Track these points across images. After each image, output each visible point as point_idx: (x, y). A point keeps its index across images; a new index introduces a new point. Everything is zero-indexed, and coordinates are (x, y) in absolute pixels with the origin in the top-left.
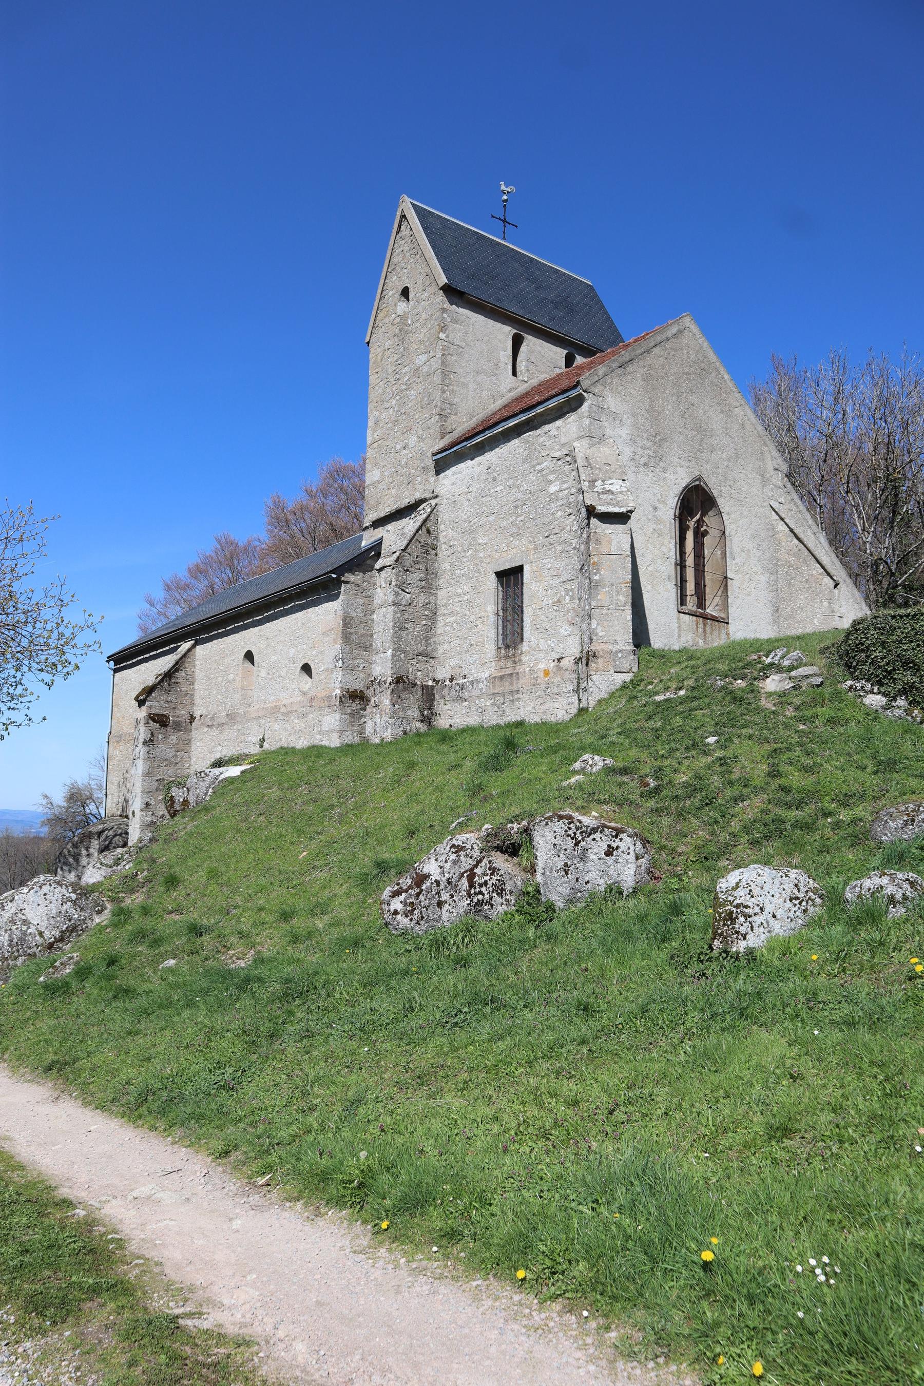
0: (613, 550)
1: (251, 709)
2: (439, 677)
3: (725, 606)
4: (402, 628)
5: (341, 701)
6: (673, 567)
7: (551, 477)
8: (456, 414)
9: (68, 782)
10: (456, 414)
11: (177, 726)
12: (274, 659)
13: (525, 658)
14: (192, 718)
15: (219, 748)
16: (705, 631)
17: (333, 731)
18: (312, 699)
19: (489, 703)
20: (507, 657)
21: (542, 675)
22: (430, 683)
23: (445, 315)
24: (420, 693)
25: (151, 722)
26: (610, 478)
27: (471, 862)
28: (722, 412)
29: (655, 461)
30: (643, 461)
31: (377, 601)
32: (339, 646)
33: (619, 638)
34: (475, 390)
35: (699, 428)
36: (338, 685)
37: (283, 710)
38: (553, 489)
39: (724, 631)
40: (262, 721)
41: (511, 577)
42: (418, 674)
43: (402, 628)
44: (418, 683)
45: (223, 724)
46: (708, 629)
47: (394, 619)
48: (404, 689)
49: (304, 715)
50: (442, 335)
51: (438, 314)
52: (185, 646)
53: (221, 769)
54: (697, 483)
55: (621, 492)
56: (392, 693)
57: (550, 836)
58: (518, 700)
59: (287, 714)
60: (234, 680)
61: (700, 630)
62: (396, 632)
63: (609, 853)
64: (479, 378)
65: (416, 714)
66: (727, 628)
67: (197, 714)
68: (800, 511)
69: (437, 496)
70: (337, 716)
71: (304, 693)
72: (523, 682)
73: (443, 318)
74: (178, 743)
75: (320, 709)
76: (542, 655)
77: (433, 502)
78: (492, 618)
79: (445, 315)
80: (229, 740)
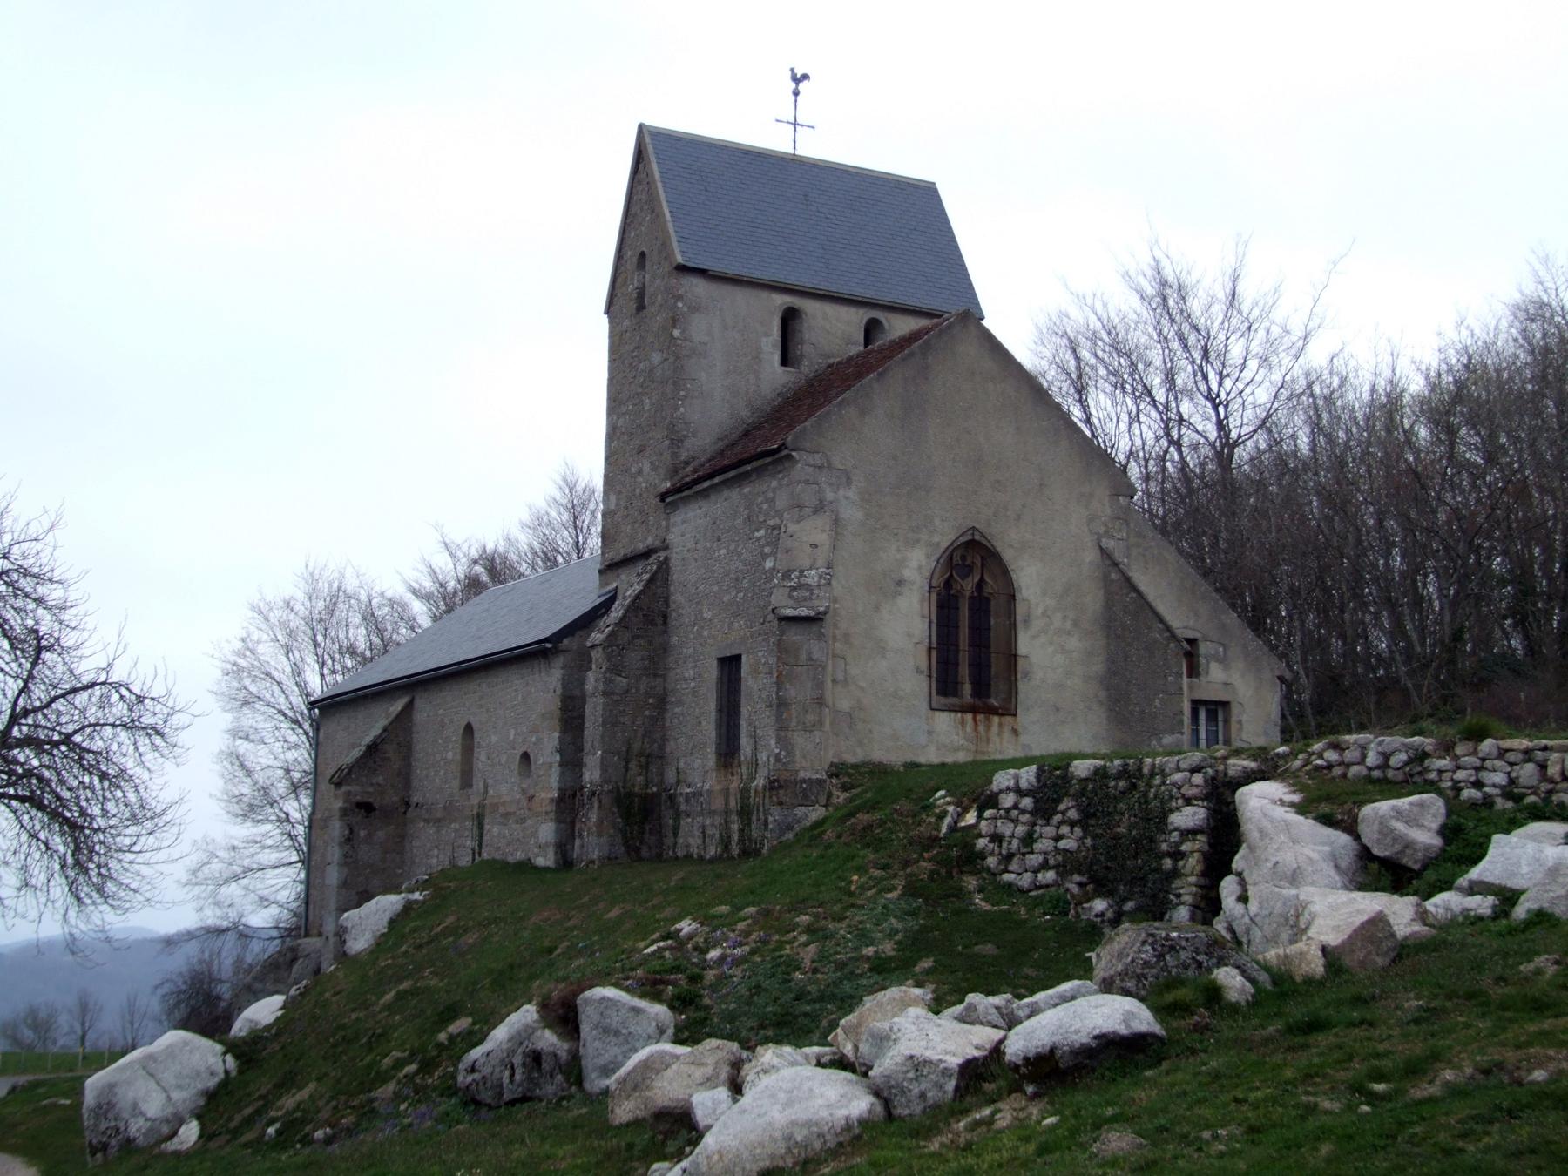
7: (767, 550)
31: (589, 687)
41: (730, 664)
43: (614, 725)
45: (439, 820)
59: (507, 815)
69: (666, 548)
77: (662, 555)
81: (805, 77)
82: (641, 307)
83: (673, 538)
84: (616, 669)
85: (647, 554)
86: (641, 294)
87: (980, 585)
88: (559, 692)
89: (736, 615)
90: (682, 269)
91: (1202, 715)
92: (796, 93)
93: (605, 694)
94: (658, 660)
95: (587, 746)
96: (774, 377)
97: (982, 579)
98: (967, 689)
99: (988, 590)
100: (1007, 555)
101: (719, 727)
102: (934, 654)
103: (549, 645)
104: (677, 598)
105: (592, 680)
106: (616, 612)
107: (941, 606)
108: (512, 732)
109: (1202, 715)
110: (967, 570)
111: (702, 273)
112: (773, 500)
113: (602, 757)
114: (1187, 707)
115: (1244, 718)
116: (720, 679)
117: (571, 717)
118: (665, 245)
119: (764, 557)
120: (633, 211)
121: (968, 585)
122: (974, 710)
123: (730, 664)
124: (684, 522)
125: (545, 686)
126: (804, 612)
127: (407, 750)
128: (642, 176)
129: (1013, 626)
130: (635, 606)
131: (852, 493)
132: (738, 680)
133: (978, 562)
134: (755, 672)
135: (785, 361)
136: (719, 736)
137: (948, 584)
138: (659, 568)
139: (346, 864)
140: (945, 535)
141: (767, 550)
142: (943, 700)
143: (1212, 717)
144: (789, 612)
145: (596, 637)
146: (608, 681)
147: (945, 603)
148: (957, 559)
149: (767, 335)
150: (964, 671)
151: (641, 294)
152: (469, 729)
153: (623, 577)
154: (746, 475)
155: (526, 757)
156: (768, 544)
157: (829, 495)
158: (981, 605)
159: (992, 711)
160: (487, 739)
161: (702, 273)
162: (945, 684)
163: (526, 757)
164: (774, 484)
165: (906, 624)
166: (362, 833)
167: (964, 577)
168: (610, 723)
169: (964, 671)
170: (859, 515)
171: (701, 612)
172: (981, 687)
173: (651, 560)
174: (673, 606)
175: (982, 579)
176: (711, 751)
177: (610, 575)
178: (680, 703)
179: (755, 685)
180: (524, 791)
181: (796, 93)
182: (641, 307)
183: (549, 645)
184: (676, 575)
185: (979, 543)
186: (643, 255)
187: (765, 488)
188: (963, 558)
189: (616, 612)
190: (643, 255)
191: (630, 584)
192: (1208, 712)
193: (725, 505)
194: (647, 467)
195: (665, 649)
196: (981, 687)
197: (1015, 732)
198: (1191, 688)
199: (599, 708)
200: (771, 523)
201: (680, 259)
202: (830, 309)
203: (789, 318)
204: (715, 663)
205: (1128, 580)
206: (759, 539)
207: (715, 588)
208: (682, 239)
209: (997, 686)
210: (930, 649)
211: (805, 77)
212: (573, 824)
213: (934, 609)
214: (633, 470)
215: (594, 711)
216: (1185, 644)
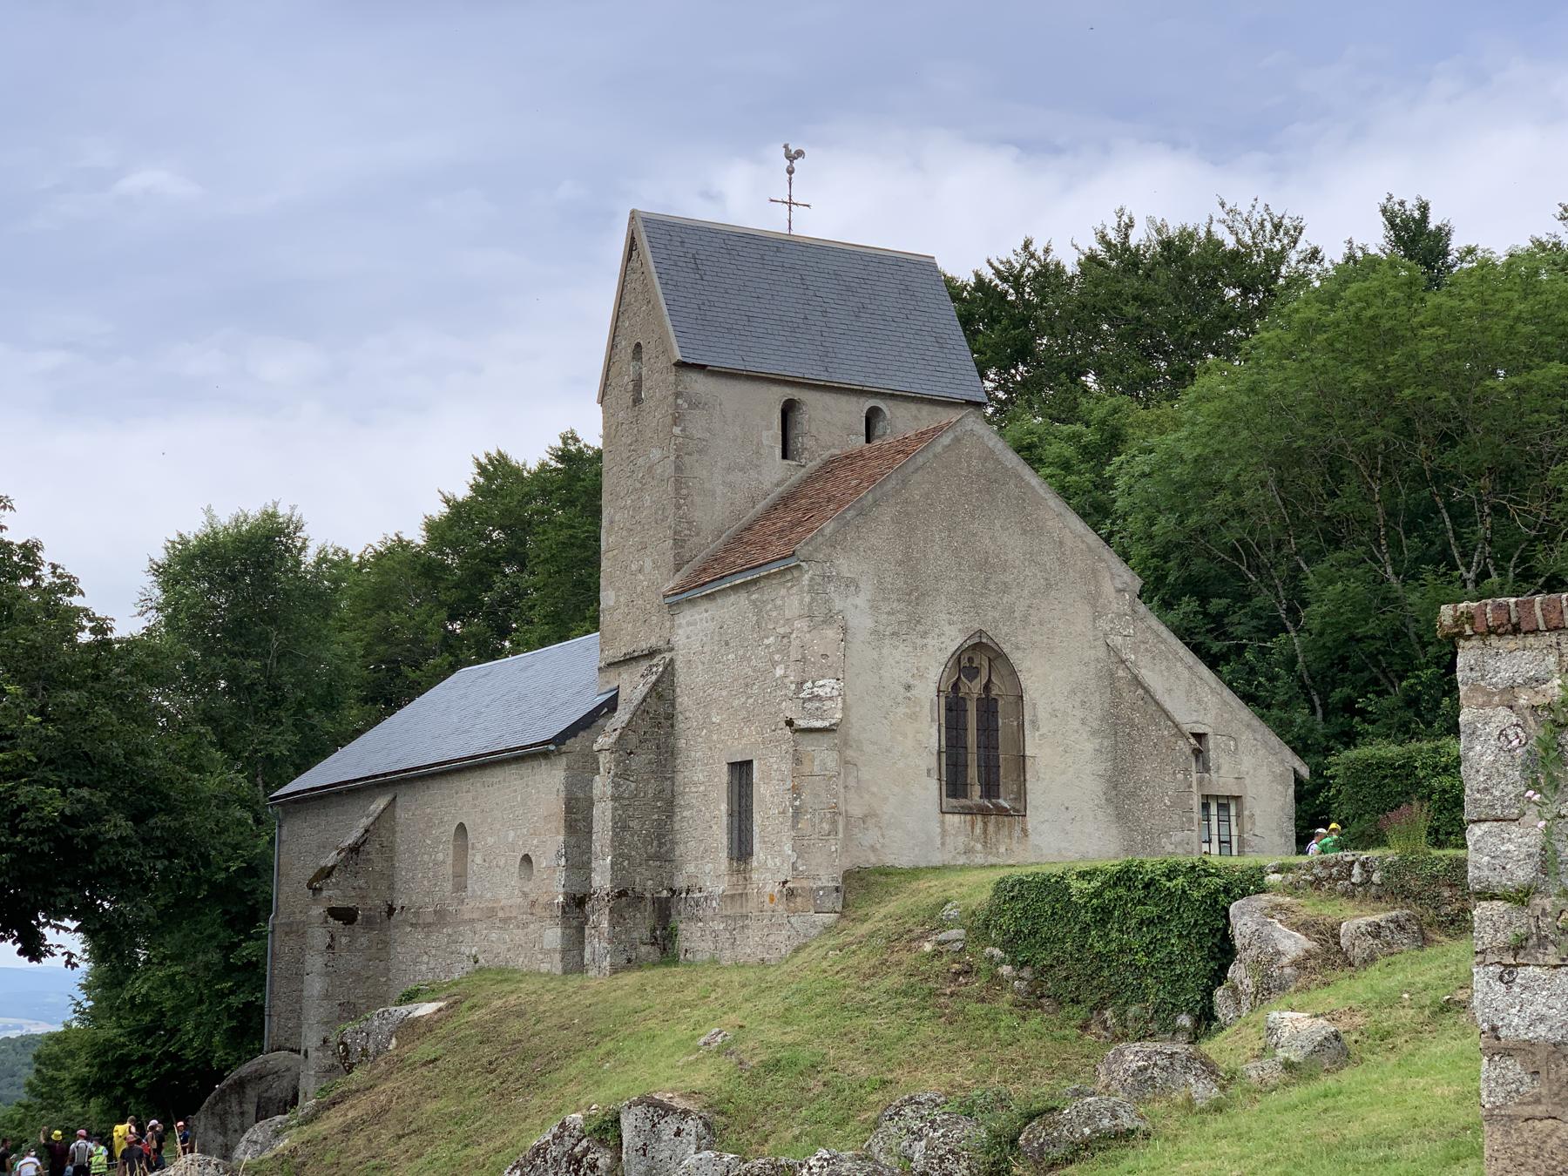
0: (816, 770)
1: (463, 908)
2: (677, 886)
3: (1021, 795)
4: (625, 828)
5: (564, 912)
6: (935, 757)
7: (777, 657)
8: (698, 534)
9: (146, 565)
10: (698, 534)
11: (369, 922)
12: (491, 841)
13: (755, 876)
14: (391, 910)
15: (425, 959)
16: (985, 831)
17: (555, 950)
18: (533, 904)
19: (722, 926)
20: (738, 871)
21: (767, 899)
22: (665, 893)
23: (680, 401)
24: (649, 908)
25: (330, 919)
26: (823, 677)
27: (573, 1141)
28: (1025, 532)
29: (913, 624)
30: (889, 630)
31: (597, 792)
32: (561, 838)
33: (821, 872)
34: (724, 495)
35: (984, 565)
36: (561, 890)
37: (501, 914)
38: (779, 672)
39: (1018, 828)
40: (478, 926)
41: (741, 770)
42: (644, 881)
43: (625, 828)
44: (648, 895)
45: (430, 925)
46: (991, 828)
47: (614, 817)
48: (629, 905)
49: (526, 925)
50: (677, 430)
51: (671, 399)
52: (380, 803)
53: (410, 1007)
54: (977, 640)
55: (831, 698)
56: (611, 911)
57: (632, 1118)
58: (747, 926)
59: (505, 921)
60: (444, 862)
61: (978, 831)
62: (616, 834)
63: (678, 1134)
64: (730, 478)
65: (646, 935)
66: (1024, 823)
67: (398, 904)
68: (1164, 641)
69: (672, 649)
70: (559, 931)
71: (525, 895)
72: (751, 906)
73: (677, 406)
74: (369, 948)
75: (542, 919)
76: (768, 875)
77: (668, 656)
78: (725, 819)
79: (680, 401)
80: (437, 948)
81: (800, 153)
82: (637, 400)
83: (679, 639)
84: (622, 775)
85: (652, 654)
86: (638, 384)
87: (987, 687)
88: (562, 795)
89: (747, 720)
90: (681, 365)
91: (1214, 809)
92: (790, 172)
93: (614, 799)
94: (666, 758)
95: (596, 847)
96: (775, 473)
97: (989, 680)
98: (976, 790)
99: (994, 692)
100: (1015, 657)
101: (730, 832)
102: (944, 756)
103: (552, 747)
104: (684, 701)
105: (602, 785)
106: (622, 716)
107: (949, 709)
108: (512, 834)
109: (1214, 809)
110: (972, 673)
111: (701, 368)
112: (781, 608)
113: (613, 864)
114: (1196, 802)
115: (1257, 812)
116: (731, 783)
117: (577, 818)
118: (663, 339)
119: (774, 664)
120: (627, 298)
121: (974, 688)
122: (984, 812)
123: (741, 770)
124: (689, 624)
125: (545, 787)
126: (819, 724)
127: (388, 852)
128: (634, 264)
129: (1021, 726)
130: (642, 710)
131: (861, 600)
132: (750, 784)
133: (986, 664)
134: (767, 778)
135: (785, 456)
136: (731, 840)
137: (956, 686)
138: (665, 668)
139: (328, 974)
140: (951, 639)
141: (777, 657)
142: (954, 802)
143: (1223, 807)
144: (802, 723)
145: (604, 741)
146: (616, 786)
147: (954, 708)
148: (965, 662)
149: (768, 428)
150: (973, 773)
151: (638, 384)
152: (461, 828)
153: (625, 676)
154: (755, 582)
155: (527, 859)
156: (778, 651)
157: (838, 604)
158: (988, 707)
159: (1002, 812)
160: (483, 840)
161: (701, 368)
162: (954, 785)
163: (527, 859)
164: (783, 592)
165: (920, 738)
166: (344, 940)
167: (971, 678)
168: (620, 827)
169: (973, 773)
170: (870, 623)
171: (709, 716)
172: (991, 790)
173: (655, 661)
174: (679, 708)
175: (989, 680)
176: (724, 855)
177: (612, 673)
178: (689, 806)
179: (768, 792)
180: (525, 895)
181: (790, 172)
182: (637, 400)
183: (552, 747)
184: (681, 678)
185: (986, 645)
186: (638, 345)
187: (773, 595)
188: (970, 660)
189: (622, 716)
190: (638, 345)
191: (633, 686)
192: (1219, 806)
193: (732, 609)
194: (648, 564)
195: (672, 753)
196: (991, 790)
197: (1024, 831)
198: (1201, 782)
199: (609, 814)
200: (781, 631)
201: (679, 357)
202: (828, 399)
203: (788, 410)
204: (726, 768)
205: (1136, 677)
206: (768, 646)
207: (724, 693)
208: (680, 334)
209: (1007, 784)
210: (939, 752)
211: (800, 153)
212: (581, 930)
213: (943, 712)
214: (634, 567)
215: (603, 816)
216: (1192, 741)
